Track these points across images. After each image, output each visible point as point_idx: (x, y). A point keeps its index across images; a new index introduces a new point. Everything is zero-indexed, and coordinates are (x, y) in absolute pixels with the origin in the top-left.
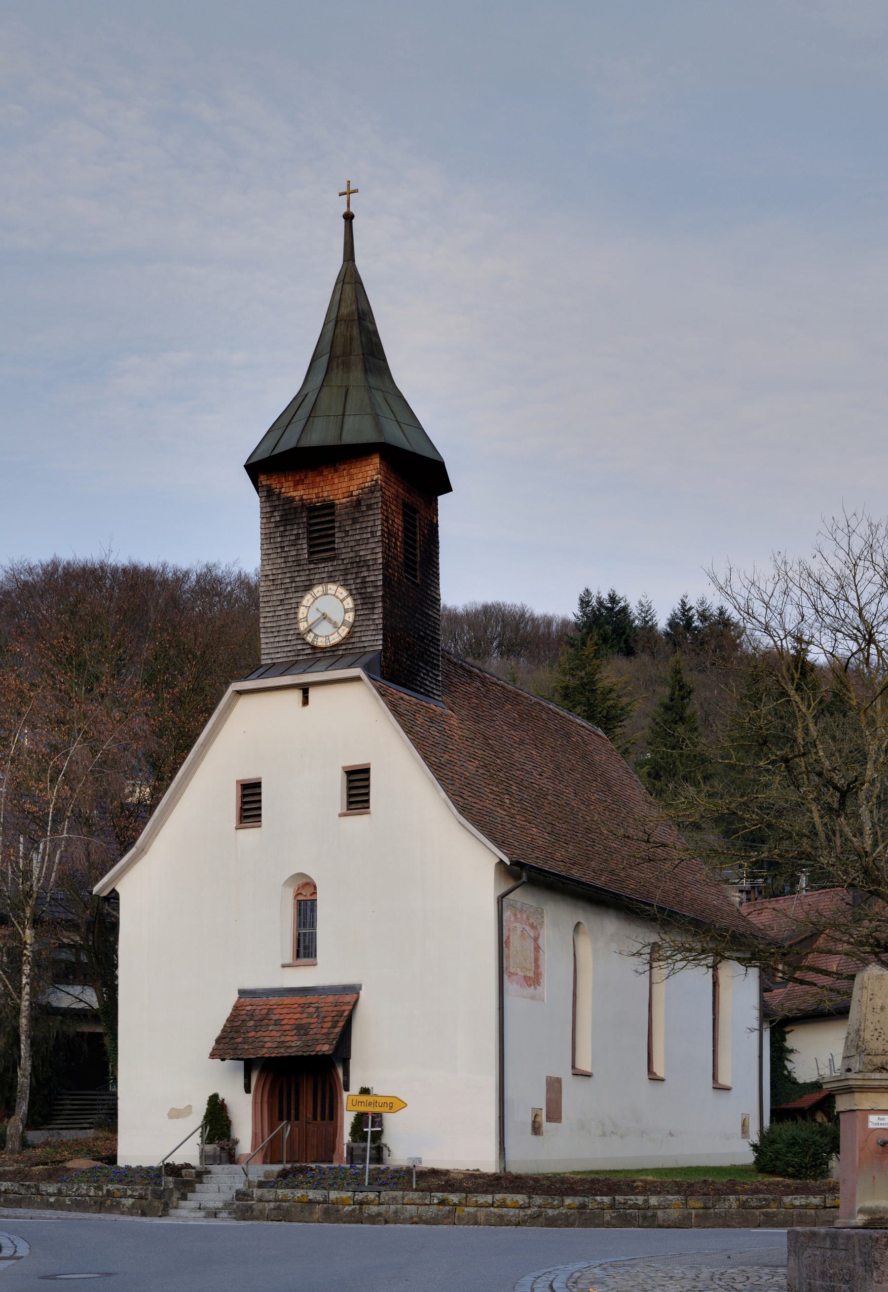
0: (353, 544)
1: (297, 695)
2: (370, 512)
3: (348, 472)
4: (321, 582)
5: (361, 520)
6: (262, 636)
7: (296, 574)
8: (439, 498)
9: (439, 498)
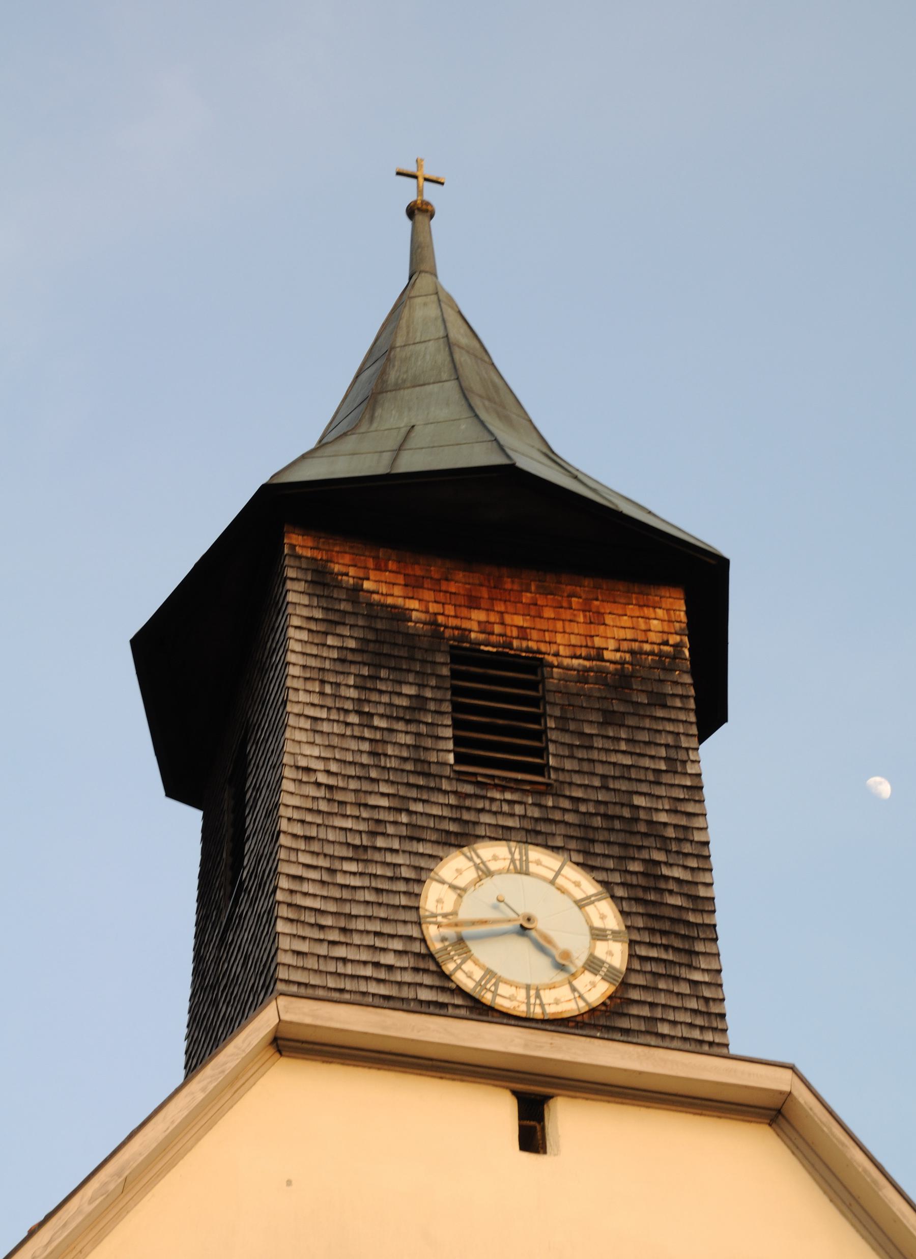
0: (610, 771)
1: (500, 1112)
2: (660, 713)
3: (587, 601)
4: (503, 834)
5: (631, 721)
6: (281, 926)
7: (413, 793)
8: (199, 814)
9: (199, 814)
